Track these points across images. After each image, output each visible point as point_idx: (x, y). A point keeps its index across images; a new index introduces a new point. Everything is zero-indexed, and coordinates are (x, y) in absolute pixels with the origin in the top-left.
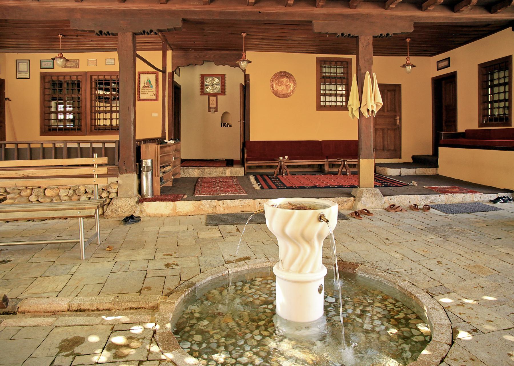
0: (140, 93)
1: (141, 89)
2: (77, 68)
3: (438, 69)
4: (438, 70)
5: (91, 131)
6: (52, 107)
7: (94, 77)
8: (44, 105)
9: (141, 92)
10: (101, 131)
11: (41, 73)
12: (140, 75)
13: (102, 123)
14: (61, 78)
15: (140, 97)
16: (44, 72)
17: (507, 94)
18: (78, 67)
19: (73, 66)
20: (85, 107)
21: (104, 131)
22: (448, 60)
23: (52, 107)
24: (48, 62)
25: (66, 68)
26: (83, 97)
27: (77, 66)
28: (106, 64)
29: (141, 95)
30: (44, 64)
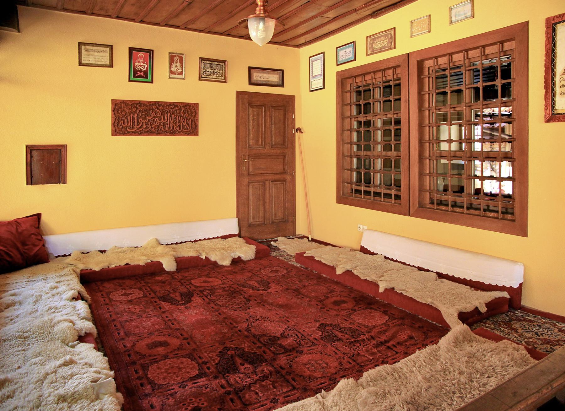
0: (554, 95)
1: (557, 79)
2: (391, 49)
3: (339, 63)
4: (338, 65)
5: (421, 205)
6: (475, 141)
7: (429, 63)
8: (343, 140)
9: (558, 90)
10: (492, 215)
11: (338, 73)
12: (554, 30)
13: (490, 187)
14: (458, 58)
15: (553, 107)
16: (341, 71)
17: (347, 127)
18: (393, 46)
19: (385, 47)
20: (408, 143)
21: (450, 208)
22: (252, 70)
23: (475, 141)
24: (346, 48)
25: (373, 54)
26: (403, 116)
27: (391, 43)
28: (451, 22)
29: (558, 99)
30: (258, 76)
